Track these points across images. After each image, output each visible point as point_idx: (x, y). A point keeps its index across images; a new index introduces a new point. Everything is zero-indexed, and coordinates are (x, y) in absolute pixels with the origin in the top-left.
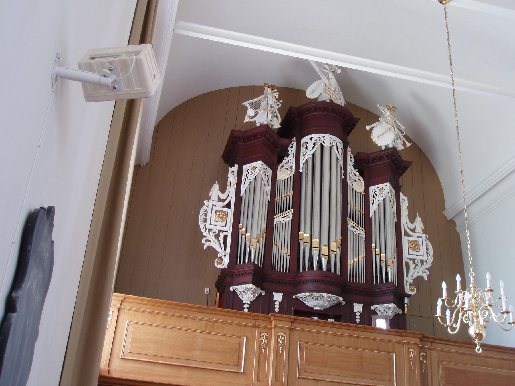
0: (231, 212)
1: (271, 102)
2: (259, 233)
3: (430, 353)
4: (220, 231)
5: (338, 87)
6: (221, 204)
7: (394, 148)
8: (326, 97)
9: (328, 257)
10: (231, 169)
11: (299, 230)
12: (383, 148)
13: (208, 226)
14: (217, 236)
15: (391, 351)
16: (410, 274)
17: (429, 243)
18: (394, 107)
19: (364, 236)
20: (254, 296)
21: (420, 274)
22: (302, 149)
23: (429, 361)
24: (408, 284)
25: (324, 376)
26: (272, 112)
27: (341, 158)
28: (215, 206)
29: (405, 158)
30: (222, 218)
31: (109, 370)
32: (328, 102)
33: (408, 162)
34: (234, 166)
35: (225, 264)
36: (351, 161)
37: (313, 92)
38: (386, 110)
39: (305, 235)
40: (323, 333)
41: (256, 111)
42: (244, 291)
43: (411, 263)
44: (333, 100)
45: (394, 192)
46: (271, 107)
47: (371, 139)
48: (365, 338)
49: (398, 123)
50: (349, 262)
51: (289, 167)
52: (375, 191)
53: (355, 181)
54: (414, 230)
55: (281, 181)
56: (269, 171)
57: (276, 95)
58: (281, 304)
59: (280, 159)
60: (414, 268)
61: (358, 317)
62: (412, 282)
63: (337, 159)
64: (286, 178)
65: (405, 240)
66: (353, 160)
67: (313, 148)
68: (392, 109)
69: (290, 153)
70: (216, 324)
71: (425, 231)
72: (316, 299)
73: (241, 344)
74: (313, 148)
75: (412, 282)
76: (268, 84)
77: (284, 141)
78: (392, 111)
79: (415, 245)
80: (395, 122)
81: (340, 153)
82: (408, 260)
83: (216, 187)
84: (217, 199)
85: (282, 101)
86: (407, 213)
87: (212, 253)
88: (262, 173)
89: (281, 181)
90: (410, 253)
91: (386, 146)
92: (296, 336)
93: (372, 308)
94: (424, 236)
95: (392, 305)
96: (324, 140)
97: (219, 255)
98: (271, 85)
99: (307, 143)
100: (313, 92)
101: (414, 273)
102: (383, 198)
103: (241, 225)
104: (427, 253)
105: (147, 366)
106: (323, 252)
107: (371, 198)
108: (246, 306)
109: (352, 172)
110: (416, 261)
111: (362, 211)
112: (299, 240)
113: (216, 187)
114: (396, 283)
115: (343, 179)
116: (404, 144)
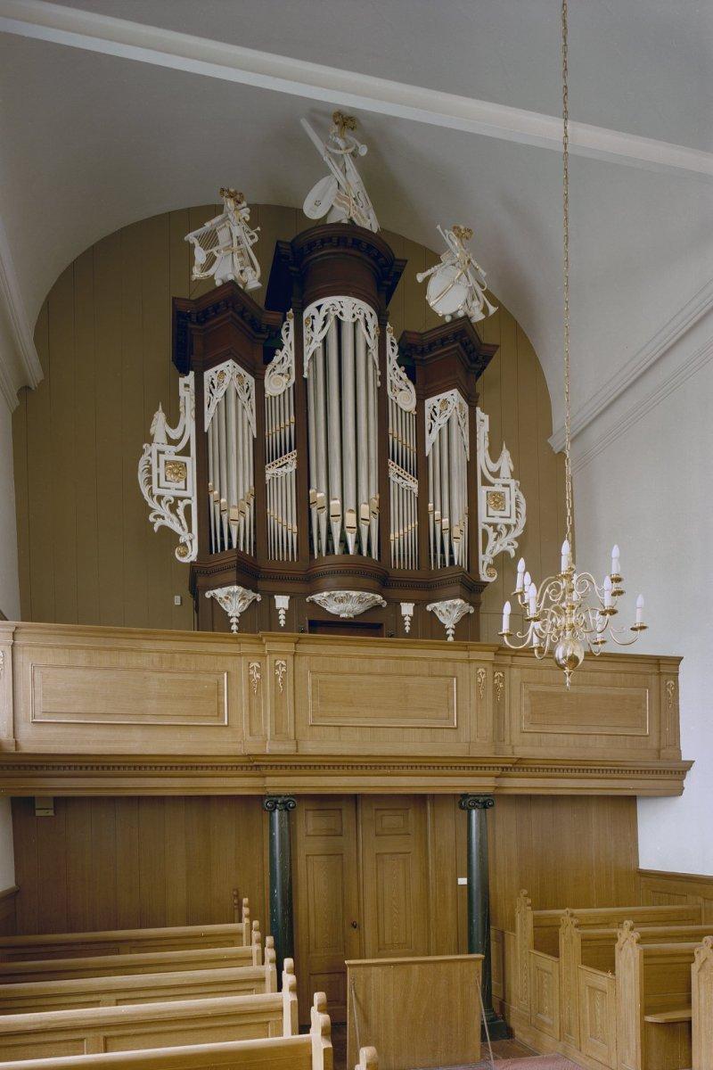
0: (191, 462)
1: (237, 231)
2: (241, 497)
3: (510, 672)
4: (177, 499)
5: (364, 189)
6: (173, 449)
7: (467, 318)
8: (340, 216)
9: (355, 530)
10: (182, 381)
11: (309, 488)
12: (448, 319)
13: (156, 491)
14: (173, 508)
15: (450, 674)
16: (489, 548)
17: (521, 496)
18: (469, 231)
19: (416, 491)
20: (244, 604)
21: (505, 547)
22: (306, 330)
23: (507, 684)
24: (486, 564)
25: (351, 720)
26: (242, 254)
27: (373, 344)
28: (163, 453)
29: (488, 338)
30: (177, 474)
31: (16, 742)
32: (345, 224)
33: (494, 346)
34: (187, 374)
35: (193, 554)
36: (393, 350)
37: (317, 203)
38: (453, 236)
39: (319, 495)
40: (346, 656)
41: (210, 251)
42: (227, 598)
43: (490, 530)
44: (355, 219)
45: (466, 407)
46: (239, 244)
47: (427, 303)
48: (410, 658)
49: (476, 264)
50: (392, 537)
51: (284, 370)
52: (435, 407)
53: (401, 390)
54: (496, 475)
55: (273, 399)
56: (250, 380)
57: (245, 213)
58: (288, 613)
59: (268, 358)
60: (496, 539)
61: (407, 623)
62: (491, 562)
63: (367, 347)
64: (281, 392)
65: (482, 491)
66: (396, 349)
67: (324, 326)
68: (464, 235)
69: (285, 341)
70: (177, 656)
71: (514, 475)
72: (341, 601)
73: (219, 685)
74: (324, 326)
75: (491, 562)
76: (228, 191)
77: (273, 317)
78: (464, 240)
79: (497, 500)
80: (469, 262)
81: (372, 335)
82: (486, 527)
83: (160, 417)
84: (165, 441)
85: (259, 229)
86: (487, 444)
87: (169, 536)
88: (235, 383)
89: (273, 399)
90: (490, 514)
91: (452, 315)
92: (303, 663)
93: (429, 608)
94: (513, 483)
95: (459, 602)
96: (342, 310)
97: (182, 540)
98: (236, 193)
99: (313, 317)
100: (317, 203)
101: (494, 548)
102: (448, 418)
103: (210, 484)
104: (517, 512)
105: (76, 730)
106: (348, 523)
107: (428, 421)
108: (450, 632)
109: (395, 373)
110: (499, 527)
111: (413, 446)
112: (309, 504)
113: (160, 417)
114: (465, 566)
115: (379, 388)
116: (485, 311)
